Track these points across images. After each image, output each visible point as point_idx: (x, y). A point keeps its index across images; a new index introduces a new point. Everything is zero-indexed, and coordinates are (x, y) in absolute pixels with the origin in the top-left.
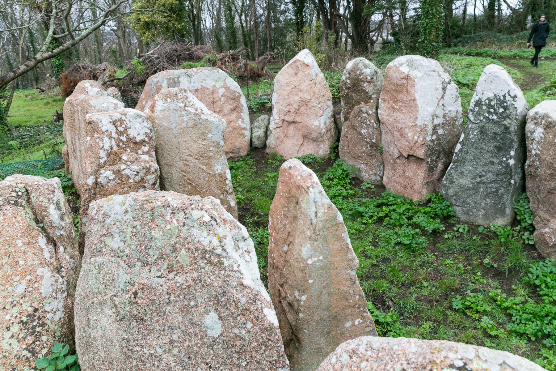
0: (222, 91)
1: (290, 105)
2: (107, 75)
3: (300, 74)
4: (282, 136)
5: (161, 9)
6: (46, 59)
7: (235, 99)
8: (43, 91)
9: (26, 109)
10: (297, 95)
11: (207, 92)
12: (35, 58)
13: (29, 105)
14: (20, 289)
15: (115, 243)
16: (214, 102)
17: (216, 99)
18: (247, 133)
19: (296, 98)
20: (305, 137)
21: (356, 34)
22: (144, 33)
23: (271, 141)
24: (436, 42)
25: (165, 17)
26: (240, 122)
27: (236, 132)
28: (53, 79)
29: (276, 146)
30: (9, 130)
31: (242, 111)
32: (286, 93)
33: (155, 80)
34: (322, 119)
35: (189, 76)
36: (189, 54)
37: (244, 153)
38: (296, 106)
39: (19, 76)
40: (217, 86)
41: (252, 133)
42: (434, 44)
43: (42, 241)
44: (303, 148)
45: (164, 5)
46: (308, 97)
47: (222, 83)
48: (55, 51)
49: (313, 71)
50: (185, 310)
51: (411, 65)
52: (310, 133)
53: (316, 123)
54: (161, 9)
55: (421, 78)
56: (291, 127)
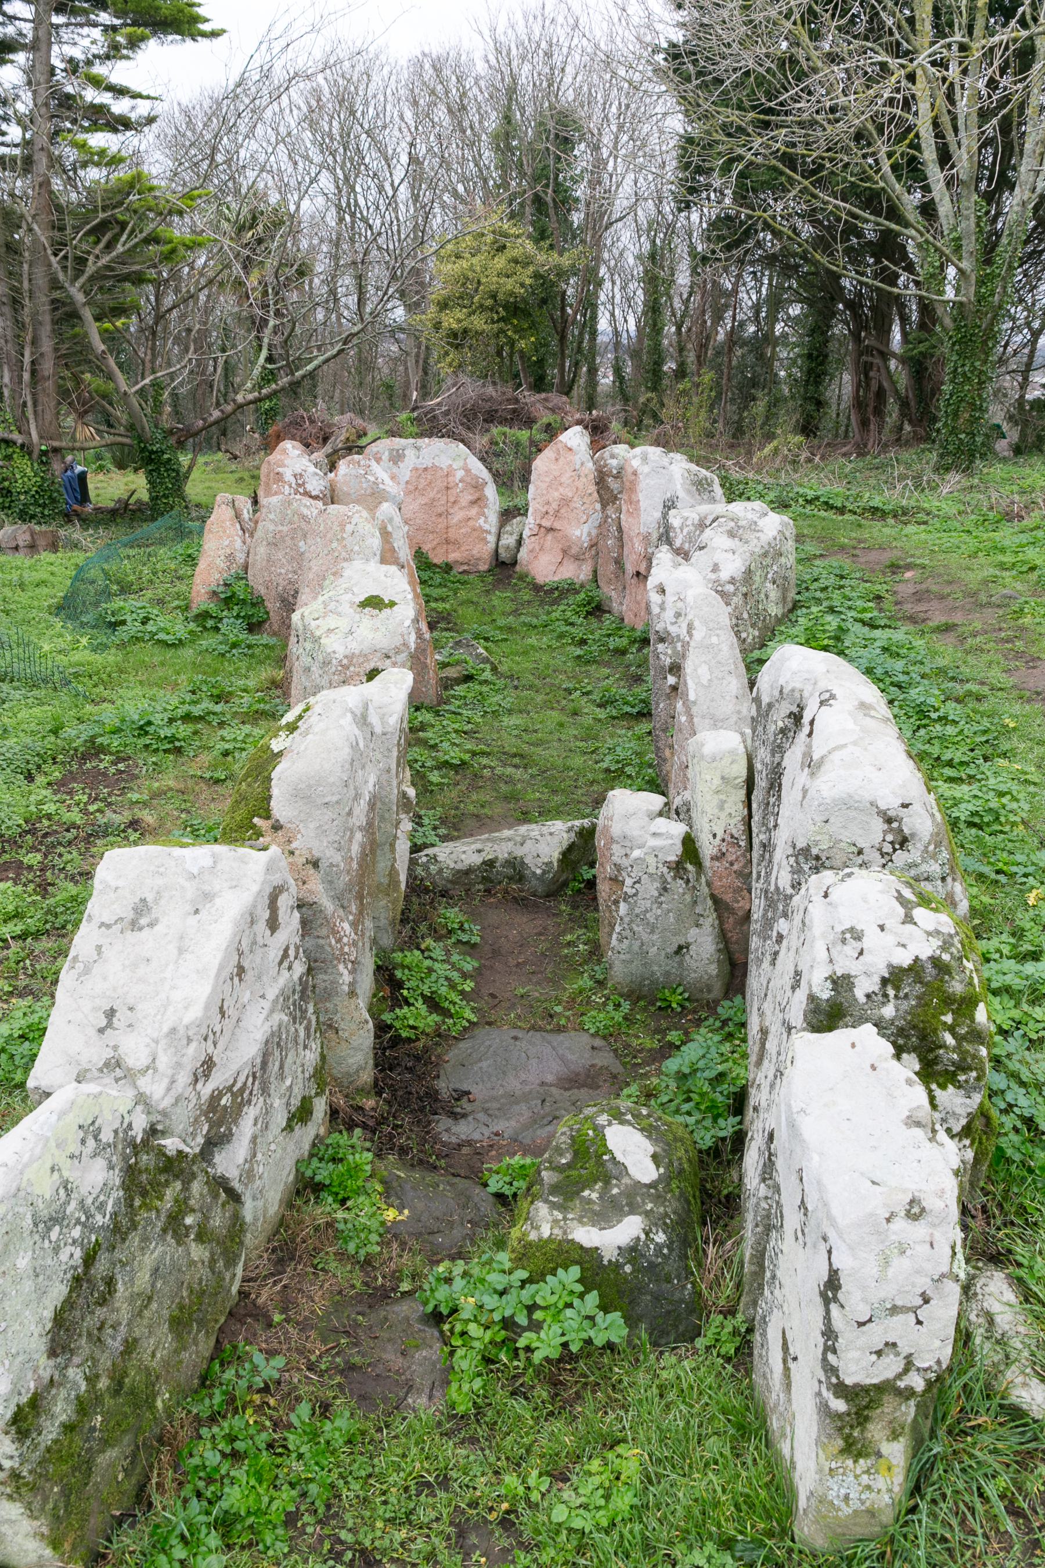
0: (460, 474)
1: (548, 503)
2: (342, 438)
3: (562, 461)
4: (537, 548)
5: (489, 302)
6: (251, 402)
7: (478, 486)
8: (235, 457)
9: (207, 484)
10: (557, 490)
11: (440, 473)
12: (234, 401)
13: (211, 480)
14: (226, 543)
15: (272, 516)
16: (448, 488)
17: (451, 485)
18: (492, 539)
19: (556, 494)
20: (565, 552)
21: (916, 396)
22: (447, 354)
23: (523, 554)
24: (968, 434)
25: (493, 322)
26: (481, 521)
27: (476, 534)
28: (256, 435)
29: (529, 563)
30: (186, 507)
31: (486, 506)
32: (544, 486)
33: (375, 450)
34: (586, 528)
35: (418, 449)
36: (514, 411)
37: (483, 567)
38: (555, 506)
39: (210, 426)
40: (455, 467)
41: (498, 540)
42: (962, 436)
43: (238, 526)
44: (561, 569)
45: (494, 296)
46: (570, 495)
47: (461, 463)
48: (264, 391)
49: (577, 457)
50: (292, 538)
51: (645, 459)
52: (570, 547)
53: (578, 533)
54: (489, 302)
55: (647, 475)
56: (549, 537)
